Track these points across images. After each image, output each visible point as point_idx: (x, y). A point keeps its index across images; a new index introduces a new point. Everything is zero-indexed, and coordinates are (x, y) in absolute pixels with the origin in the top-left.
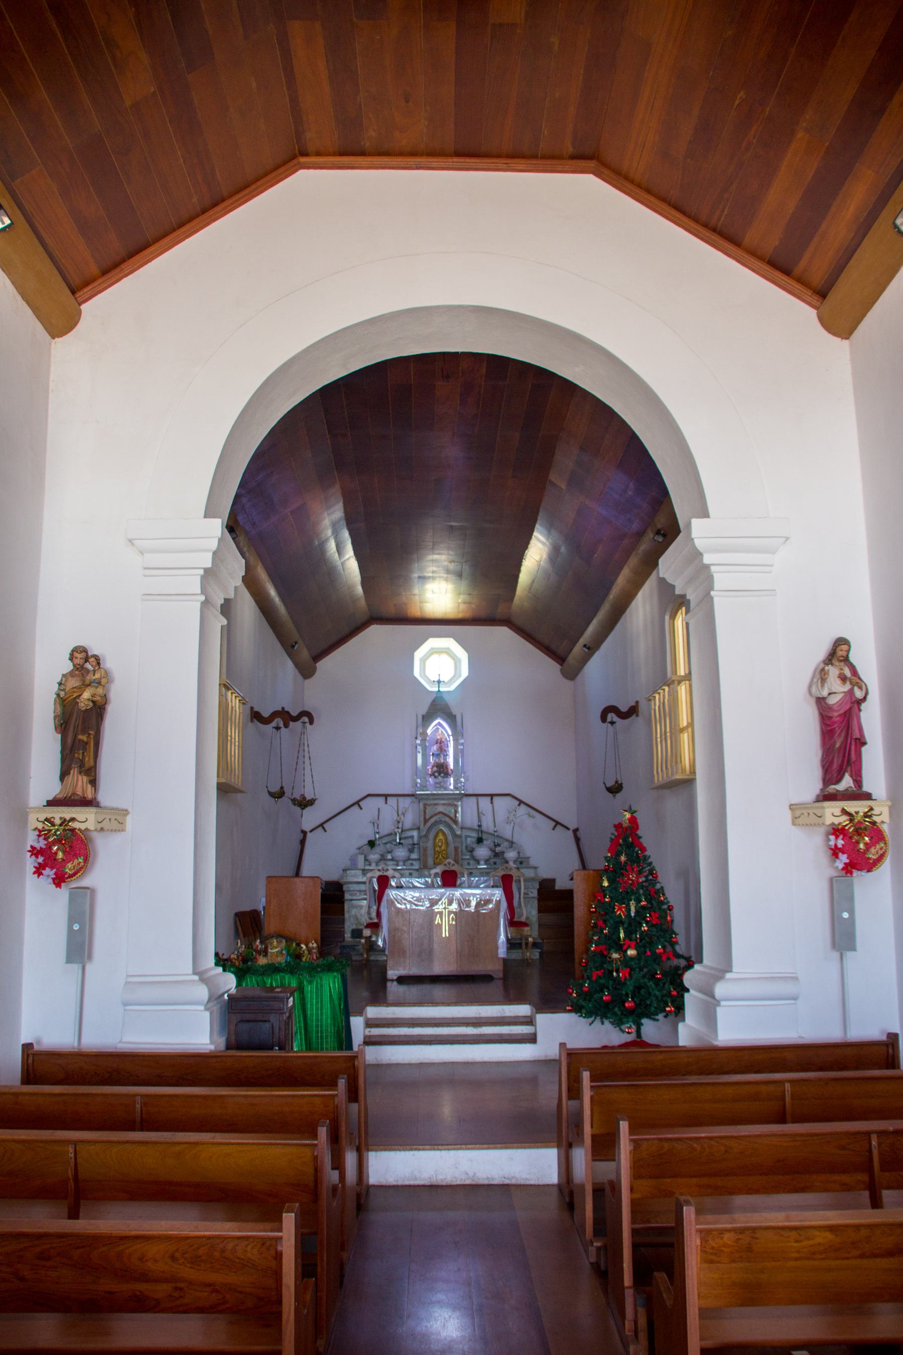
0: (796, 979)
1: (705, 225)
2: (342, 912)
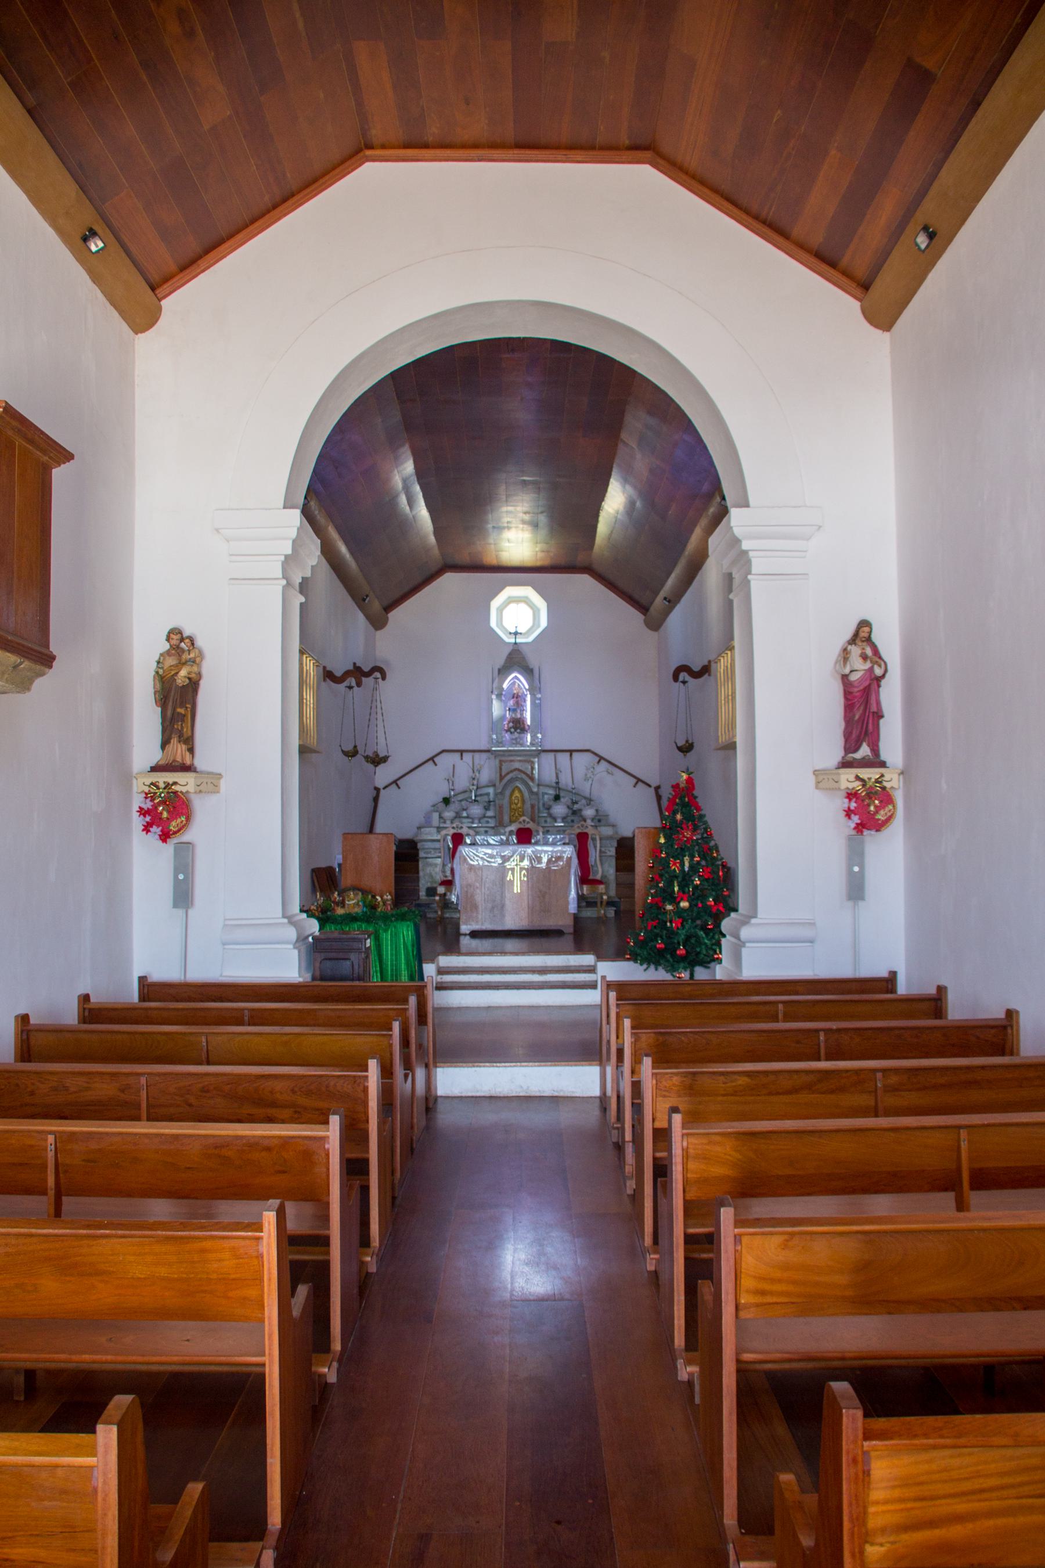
0: (813, 924)
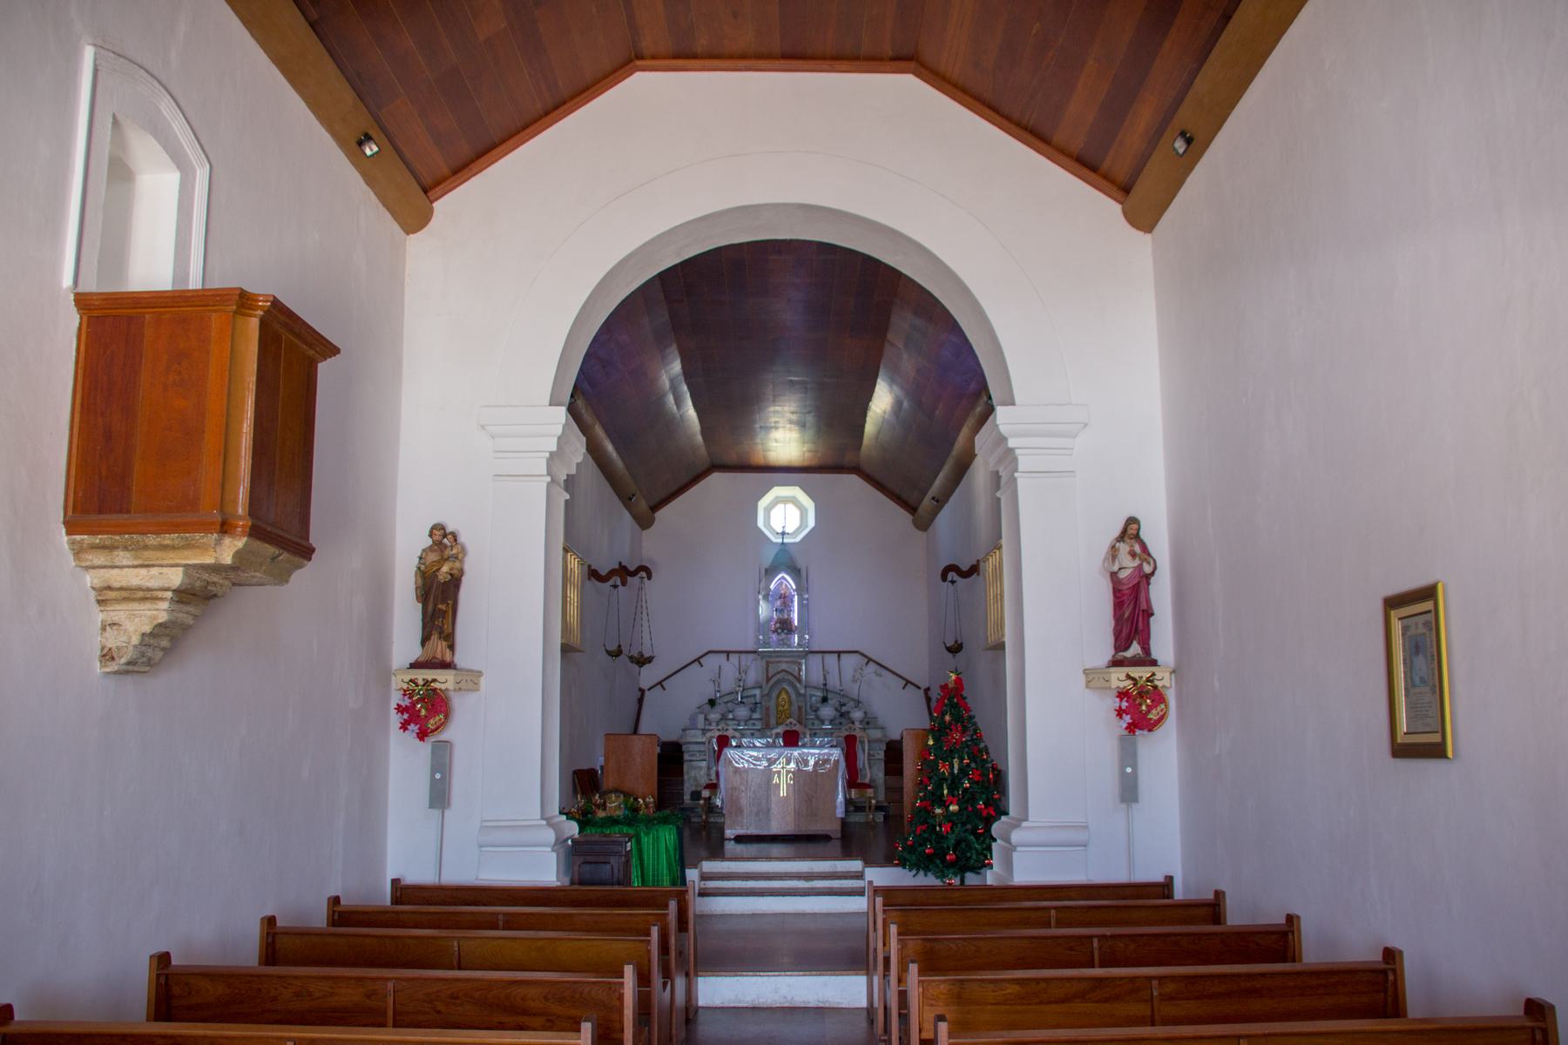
1: (1018, 124)
2: (682, 774)
